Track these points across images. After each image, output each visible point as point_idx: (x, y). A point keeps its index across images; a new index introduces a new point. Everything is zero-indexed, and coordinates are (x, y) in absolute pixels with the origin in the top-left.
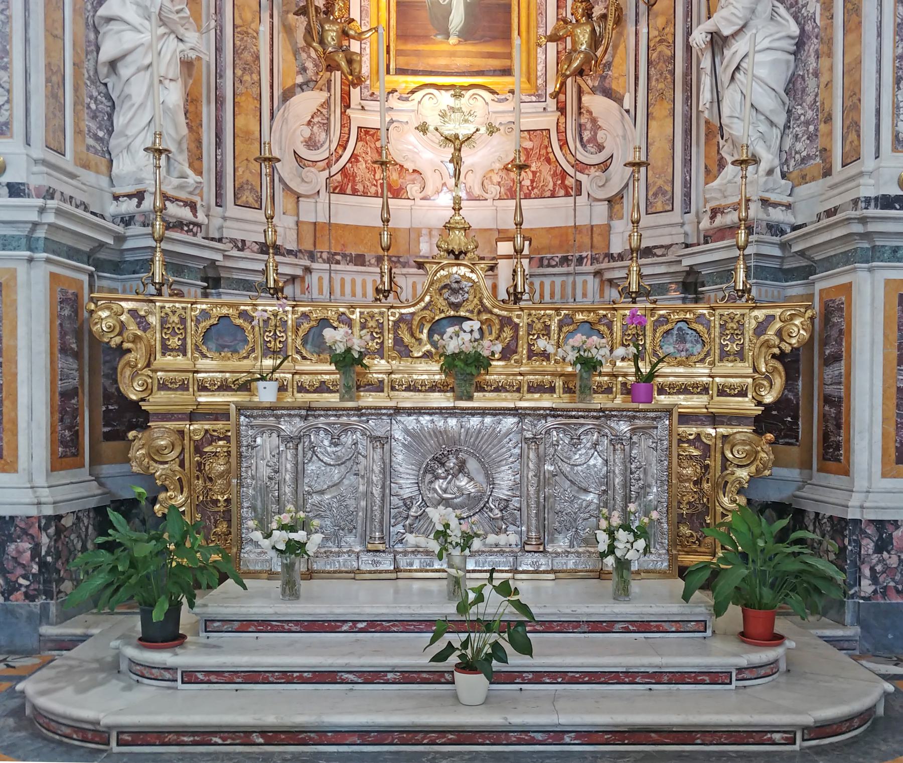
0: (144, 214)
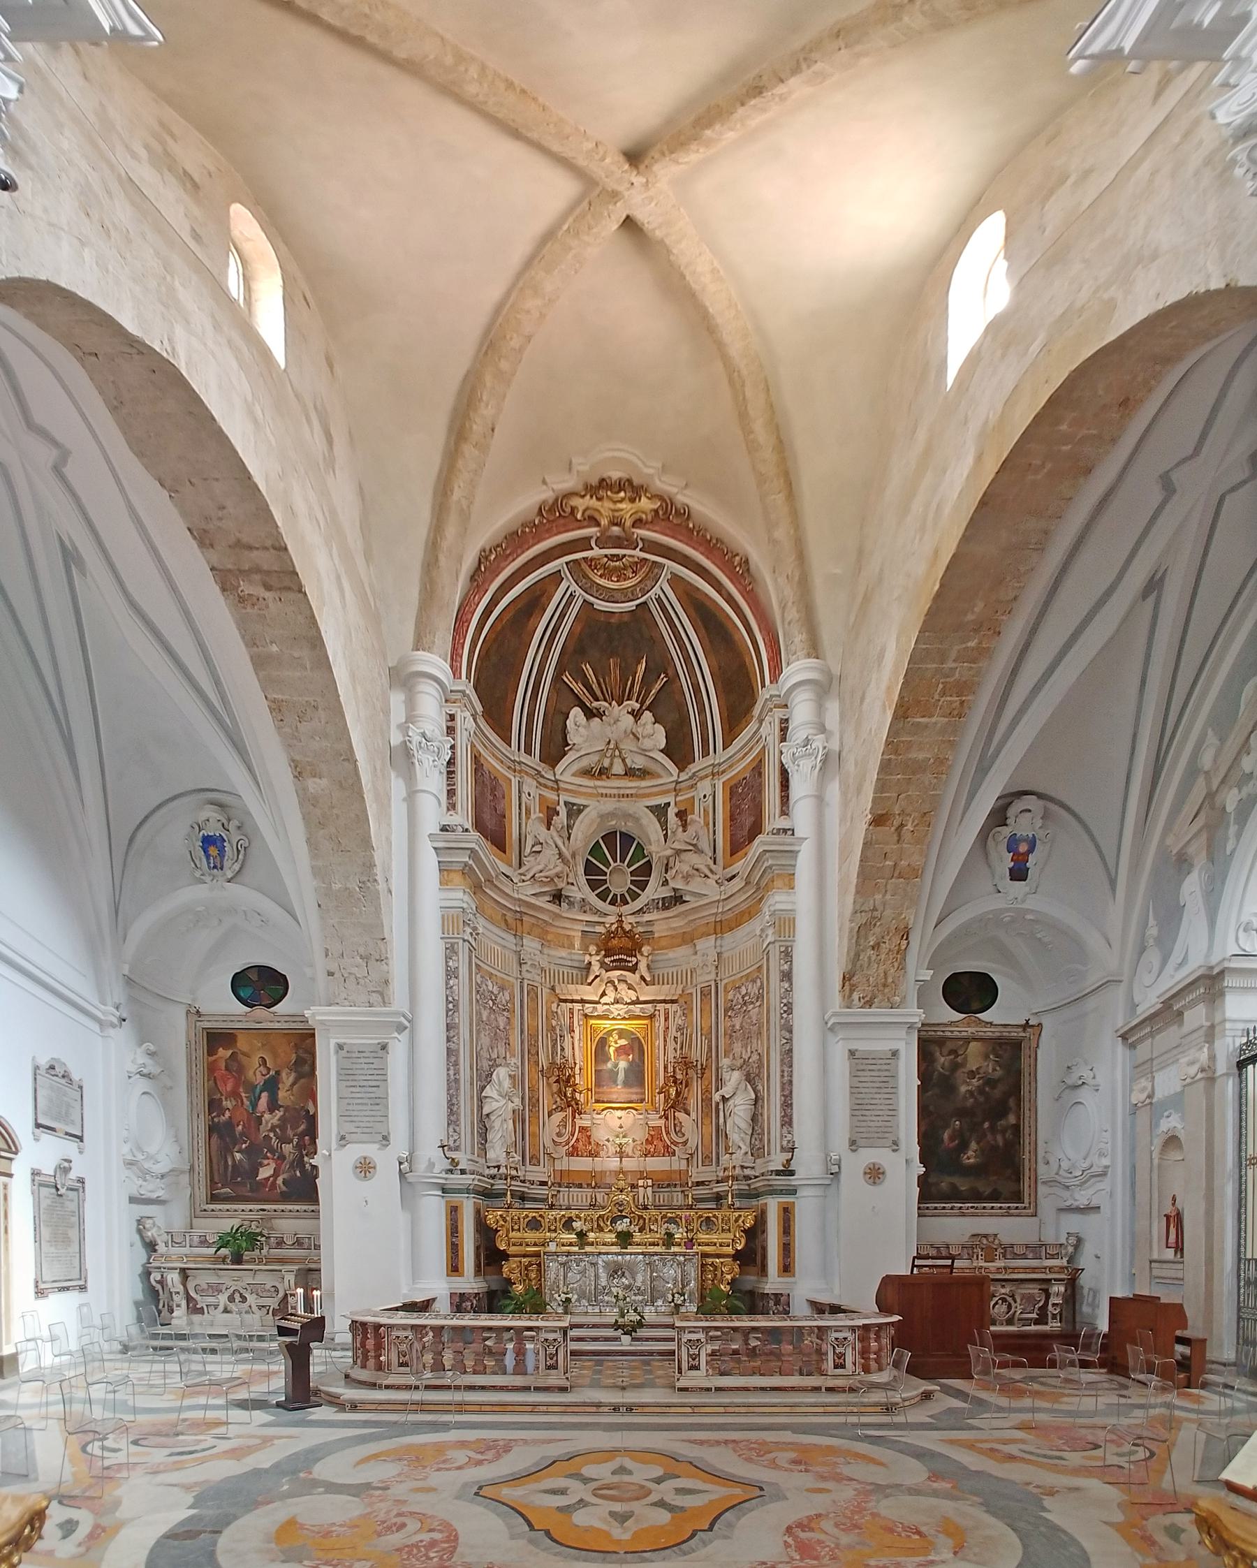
0: (501, 1175)
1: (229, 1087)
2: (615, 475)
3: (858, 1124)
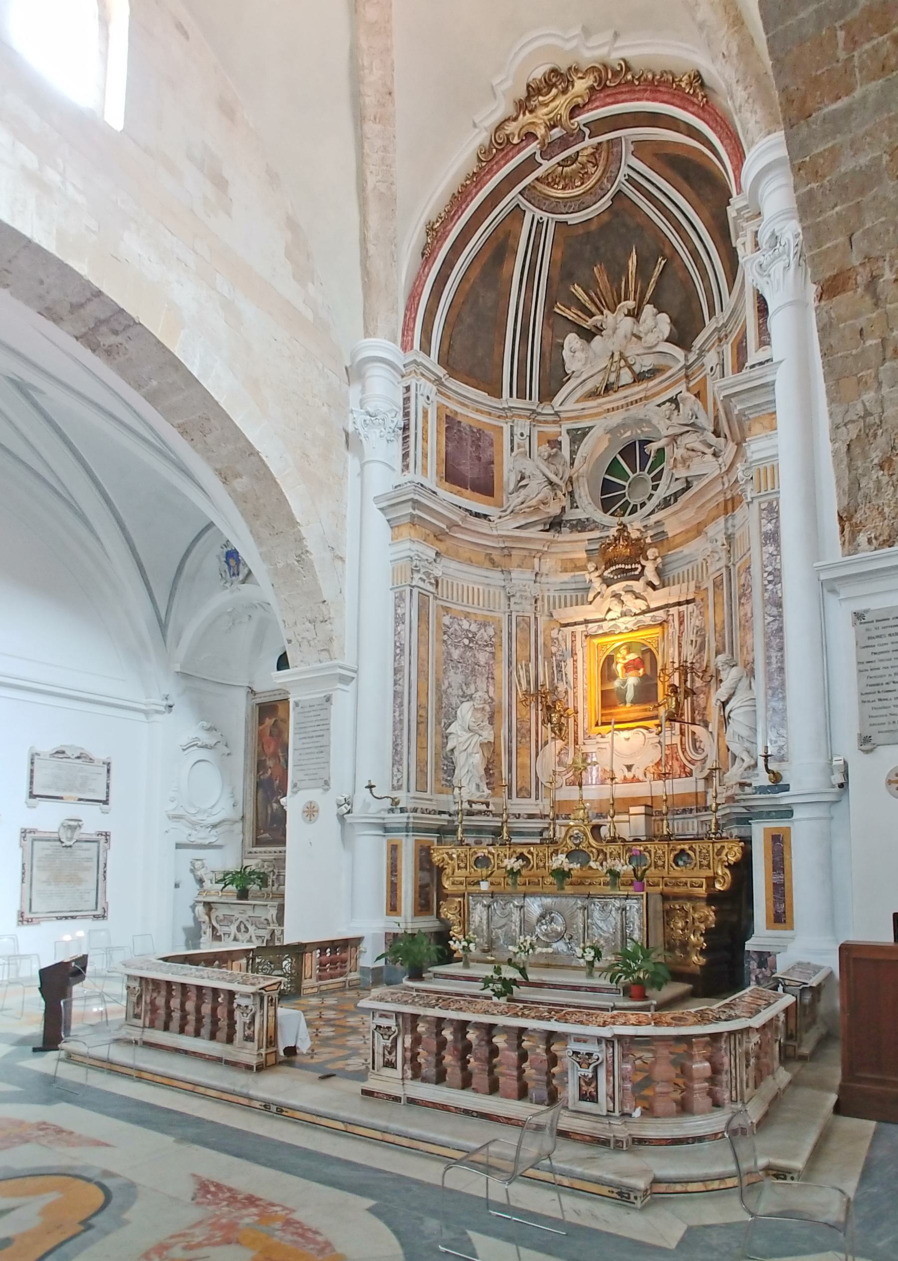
1: (272, 748)
2: (539, 73)
3: (874, 713)
